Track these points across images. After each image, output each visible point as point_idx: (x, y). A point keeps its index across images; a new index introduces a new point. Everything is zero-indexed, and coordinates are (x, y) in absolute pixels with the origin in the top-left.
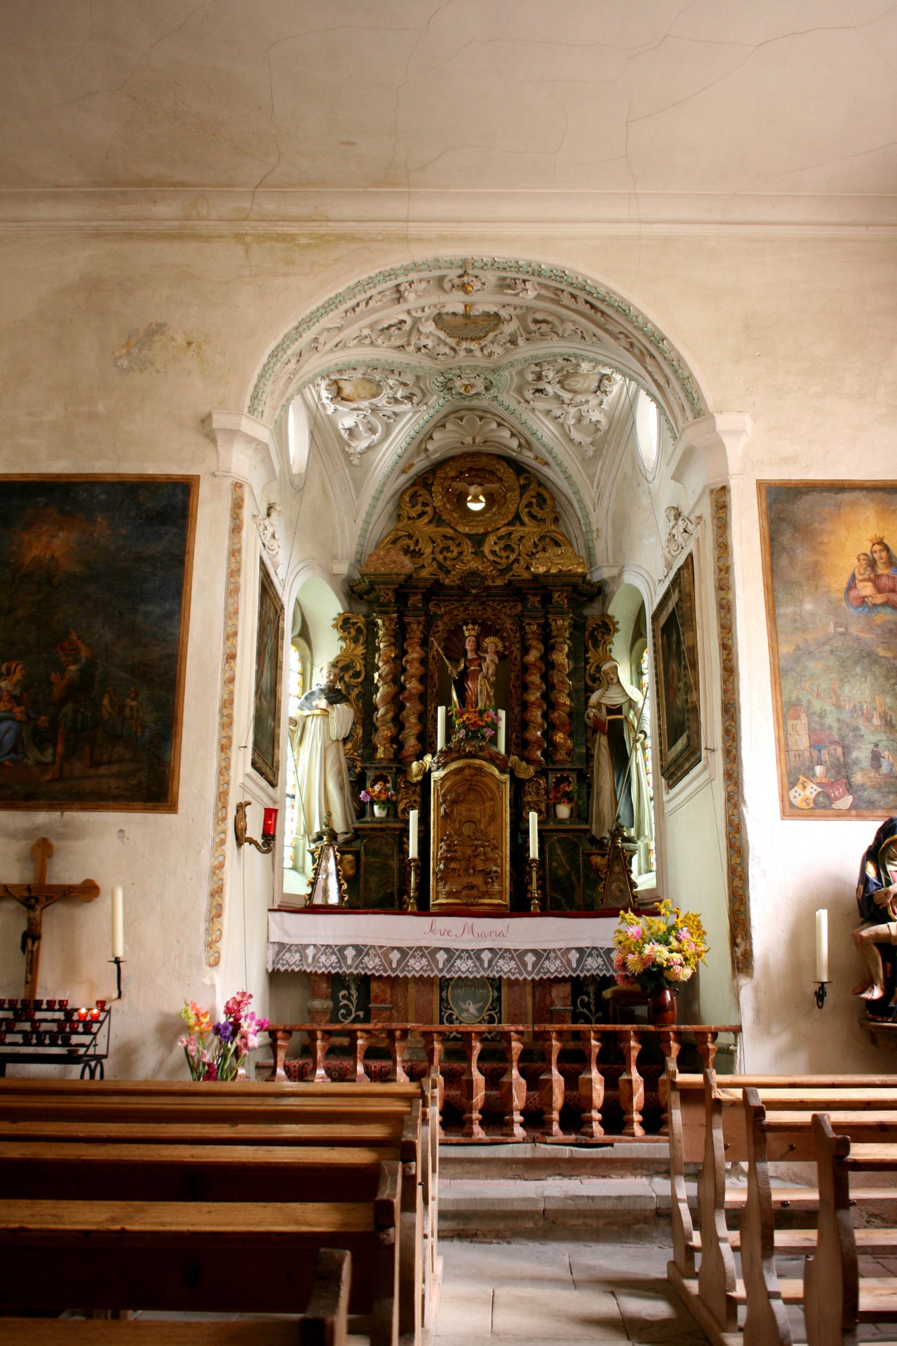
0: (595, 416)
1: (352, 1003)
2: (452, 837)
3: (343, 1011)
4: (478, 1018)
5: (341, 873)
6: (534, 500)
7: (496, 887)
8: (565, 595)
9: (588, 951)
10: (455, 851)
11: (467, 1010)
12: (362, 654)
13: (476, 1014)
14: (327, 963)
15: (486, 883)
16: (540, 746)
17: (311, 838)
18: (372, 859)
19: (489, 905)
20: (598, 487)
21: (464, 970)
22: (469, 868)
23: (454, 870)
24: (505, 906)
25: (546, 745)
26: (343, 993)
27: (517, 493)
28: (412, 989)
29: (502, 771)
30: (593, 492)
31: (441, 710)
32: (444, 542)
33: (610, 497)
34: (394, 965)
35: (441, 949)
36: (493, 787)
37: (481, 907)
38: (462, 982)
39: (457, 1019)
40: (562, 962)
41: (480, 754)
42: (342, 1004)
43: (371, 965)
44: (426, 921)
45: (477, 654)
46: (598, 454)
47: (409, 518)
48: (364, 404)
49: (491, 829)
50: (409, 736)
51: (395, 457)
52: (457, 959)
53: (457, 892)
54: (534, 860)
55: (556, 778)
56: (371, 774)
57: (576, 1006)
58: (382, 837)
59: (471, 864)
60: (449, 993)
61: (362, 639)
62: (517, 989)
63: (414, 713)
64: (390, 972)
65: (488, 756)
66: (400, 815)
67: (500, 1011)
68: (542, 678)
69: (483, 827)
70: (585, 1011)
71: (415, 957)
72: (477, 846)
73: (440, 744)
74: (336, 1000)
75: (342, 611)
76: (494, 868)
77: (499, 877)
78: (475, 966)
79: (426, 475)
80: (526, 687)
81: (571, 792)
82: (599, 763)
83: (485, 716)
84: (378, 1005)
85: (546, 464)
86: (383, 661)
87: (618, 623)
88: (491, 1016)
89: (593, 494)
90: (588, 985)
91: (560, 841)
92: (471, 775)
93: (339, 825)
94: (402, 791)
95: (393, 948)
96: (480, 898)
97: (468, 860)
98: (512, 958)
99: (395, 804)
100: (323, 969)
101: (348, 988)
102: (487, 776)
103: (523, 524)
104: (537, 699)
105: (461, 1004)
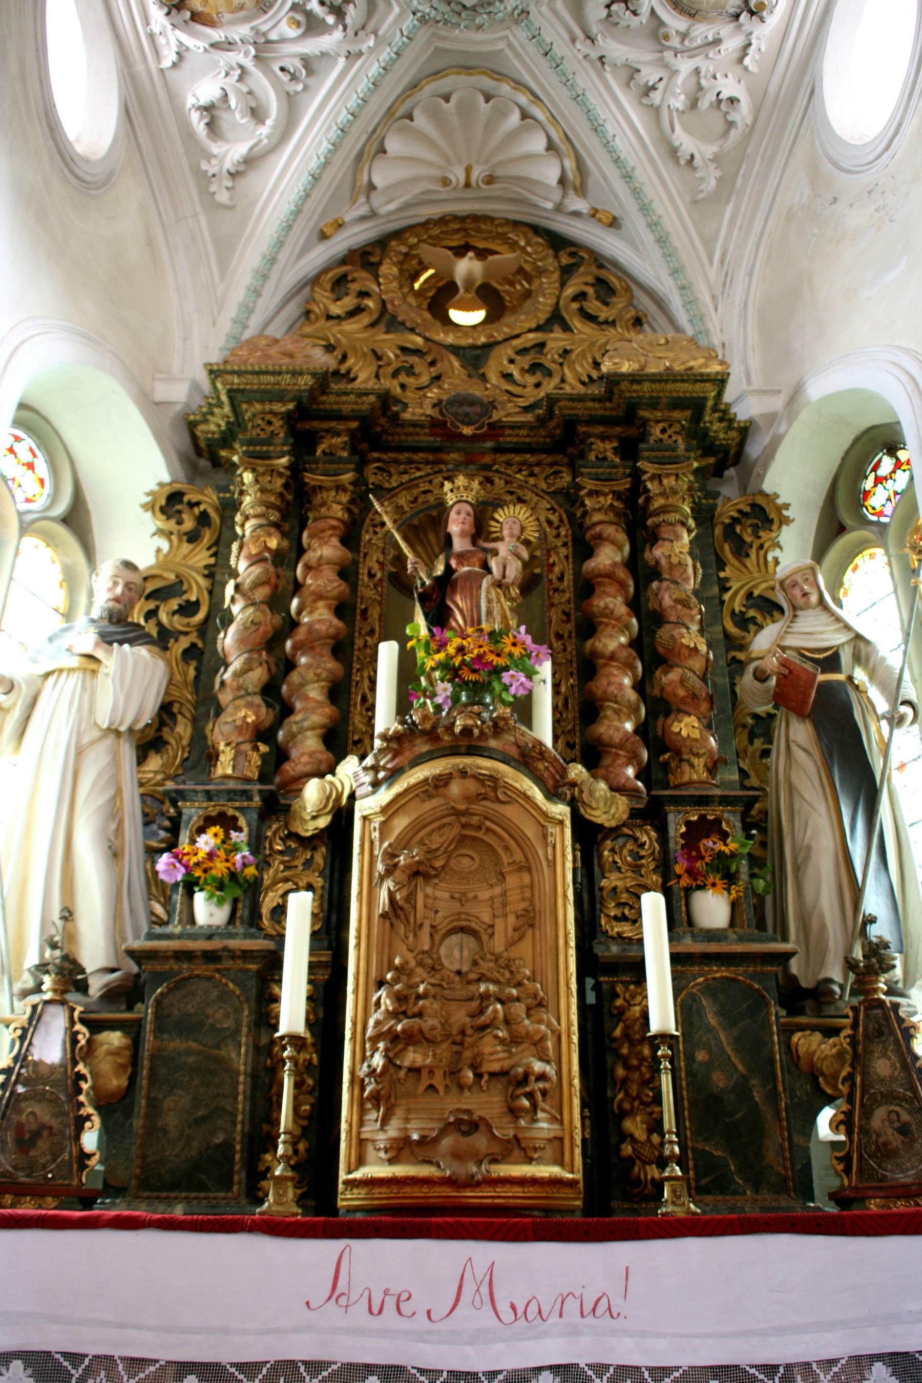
0: (729, 87)
2: (410, 974)
6: (590, 291)
7: (544, 1126)
8: (677, 427)
10: (420, 1015)
12: (207, 567)
15: (514, 1112)
16: (633, 758)
17: (18, 986)
18: (175, 1044)
19: (522, 1182)
20: (722, 262)
22: (460, 1062)
23: (415, 1071)
24: (572, 1184)
25: (645, 755)
27: (556, 275)
29: (552, 795)
30: (713, 273)
31: (387, 653)
32: (403, 358)
33: (750, 275)
36: (531, 832)
37: (500, 1190)
41: (493, 743)
44: (323, 1251)
45: (474, 543)
46: (726, 186)
47: (329, 317)
48: (241, 31)
49: (524, 949)
50: (302, 730)
51: (305, 179)
54: (664, 1037)
55: (688, 824)
56: (192, 812)
58: (209, 979)
59: (468, 1054)
61: (207, 537)
63: (319, 678)
65: (514, 752)
66: (266, 922)
68: (628, 604)
69: (498, 944)
72: (485, 997)
73: (385, 719)
75: (167, 478)
76: (538, 1067)
77: (554, 1093)
79: (369, 249)
81: (733, 855)
82: (791, 789)
83: (507, 641)
85: (614, 223)
86: (249, 557)
87: (787, 506)
89: (712, 276)
91: (710, 989)
92: (469, 799)
93: (95, 953)
94: (277, 864)
96: (495, 1161)
97: (459, 1040)
99: (254, 889)
102: (510, 801)
103: (567, 328)
104: (622, 646)
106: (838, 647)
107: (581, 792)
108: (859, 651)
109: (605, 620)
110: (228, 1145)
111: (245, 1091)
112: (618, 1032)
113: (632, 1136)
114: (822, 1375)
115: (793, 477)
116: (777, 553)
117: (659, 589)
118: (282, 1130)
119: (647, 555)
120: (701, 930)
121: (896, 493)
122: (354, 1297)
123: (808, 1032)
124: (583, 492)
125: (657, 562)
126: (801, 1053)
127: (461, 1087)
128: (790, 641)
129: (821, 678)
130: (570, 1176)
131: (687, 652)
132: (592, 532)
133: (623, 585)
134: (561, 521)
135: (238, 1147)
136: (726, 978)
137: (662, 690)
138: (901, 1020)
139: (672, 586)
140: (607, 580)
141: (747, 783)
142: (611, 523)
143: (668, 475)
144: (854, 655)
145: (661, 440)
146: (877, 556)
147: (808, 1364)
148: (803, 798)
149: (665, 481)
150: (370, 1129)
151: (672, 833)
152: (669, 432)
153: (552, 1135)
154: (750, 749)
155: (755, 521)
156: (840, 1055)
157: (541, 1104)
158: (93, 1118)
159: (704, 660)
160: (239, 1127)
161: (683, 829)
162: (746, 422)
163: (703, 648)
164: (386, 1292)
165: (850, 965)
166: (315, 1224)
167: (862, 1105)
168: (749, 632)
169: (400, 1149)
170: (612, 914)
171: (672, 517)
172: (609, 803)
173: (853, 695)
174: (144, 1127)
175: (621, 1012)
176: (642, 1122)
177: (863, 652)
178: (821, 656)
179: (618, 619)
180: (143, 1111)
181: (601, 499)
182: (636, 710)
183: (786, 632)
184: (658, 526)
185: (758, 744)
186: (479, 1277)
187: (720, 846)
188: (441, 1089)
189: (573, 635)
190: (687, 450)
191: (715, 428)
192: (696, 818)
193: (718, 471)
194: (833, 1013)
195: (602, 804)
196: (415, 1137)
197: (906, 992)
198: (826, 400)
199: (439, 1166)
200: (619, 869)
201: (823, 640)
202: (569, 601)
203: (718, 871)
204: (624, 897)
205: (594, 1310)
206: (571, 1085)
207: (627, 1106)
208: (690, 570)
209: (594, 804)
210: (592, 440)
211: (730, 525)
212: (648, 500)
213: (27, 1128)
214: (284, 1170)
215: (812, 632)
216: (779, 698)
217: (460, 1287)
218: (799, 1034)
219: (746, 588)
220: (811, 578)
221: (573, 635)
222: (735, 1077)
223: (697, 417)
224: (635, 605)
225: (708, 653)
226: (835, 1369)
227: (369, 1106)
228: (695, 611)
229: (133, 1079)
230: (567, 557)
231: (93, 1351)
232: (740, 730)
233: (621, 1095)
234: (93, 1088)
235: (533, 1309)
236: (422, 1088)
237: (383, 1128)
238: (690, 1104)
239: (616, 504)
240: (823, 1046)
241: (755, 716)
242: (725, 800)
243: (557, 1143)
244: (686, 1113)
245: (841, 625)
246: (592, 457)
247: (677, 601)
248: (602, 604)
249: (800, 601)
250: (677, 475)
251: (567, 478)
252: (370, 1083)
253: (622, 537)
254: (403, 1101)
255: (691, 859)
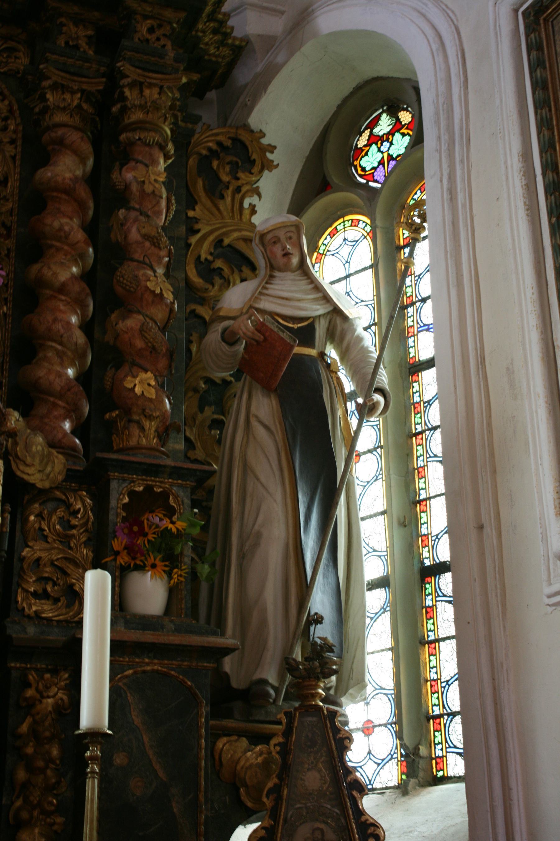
8: (167, 30)
16: (72, 411)
54: (94, 735)
55: (132, 494)
80: (34, 248)
81: (179, 535)
82: (246, 468)
87: (272, 148)
104: (73, 276)
106: (314, 318)
107: (16, 444)
108: (335, 327)
109: (58, 244)
112: (24, 728)
115: (283, 117)
116: (254, 200)
117: (125, 218)
119: (115, 176)
120: (135, 615)
121: (390, 158)
123: (234, 738)
124: (46, 83)
125: (127, 187)
126: (224, 761)
128: (265, 304)
129: (298, 350)
131: (150, 299)
132: (53, 135)
133: (82, 206)
134: (11, 111)
136: (157, 671)
137: (117, 337)
138: (336, 730)
139: (143, 218)
140: (64, 196)
141: (191, 454)
142: (76, 128)
143: (150, 86)
144: (328, 329)
145: (147, 41)
146: (361, 225)
148: (258, 479)
149: (147, 92)
151: (113, 503)
152: (158, 33)
154: (200, 417)
155: (235, 159)
156: (266, 764)
159: (168, 310)
161: (126, 500)
162: (242, 40)
163: (169, 297)
165: (288, 665)
168: (213, 285)
170: (32, 589)
171: (152, 137)
172: (46, 460)
173: (323, 373)
175: (31, 704)
176: (41, 834)
177: (339, 328)
178: (296, 326)
179: (73, 245)
181: (68, 96)
182: (83, 356)
183: (261, 293)
184: (132, 144)
185: (209, 412)
187: (166, 523)
189: (13, 254)
190: (176, 60)
191: (207, 40)
192: (141, 488)
193: (198, 91)
194: (262, 718)
195: (37, 461)
197: (338, 701)
198: (336, 35)
200: (45, 538)
201: (300, 309)
202: (11, 212)
203: (159, 551)
204: (48, 571)
207: (25, 815)
208: (164, 203)
209: (29, 460)
210: (63, 20)
211: (206, 156)
212: (124, 110)
215: (286, 298)
216: (245, 368)
218: (225, 739)
219: (216, 234)
220: (295, 237)
221: (13, 254)
223: (190, 24)
224: (92, 230)
225: (173, 303)
228: (163, 253)
230: (14, 158)
232: (190, 394)
239: (85, 106)
240: (249, 753)
241: (209, 381)
242: (176, 473)
245: (320, 295)
246: (61, 42)
247: (146, 237)
248: (56, 224)
249: (281, 261)
250: (161, 88)
251: (22, 61)
253: (87, 148)
255: (131, 534)
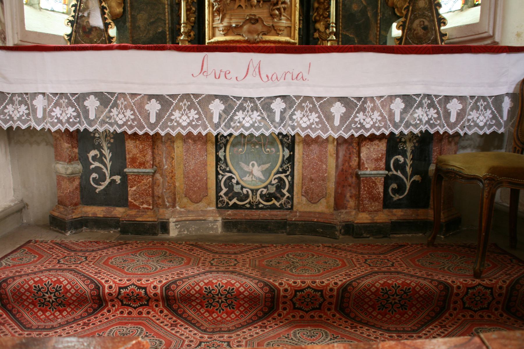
1: (105, 165)
3: (94, 175)
4: (263, 182)
5: (106, 12)
7: (284, 22)
9: (418, 100)
11: (251, 173)
13: (262, 177)
14: (63, 118)
15: (272, 16)
19: (274, 42)
21: (247, 125)
26: (93, 153)
28: (179, 148)
34: (153, 120)
35: (216, 96)
38: (244, 140)
39: (238, 183)
40: (381, 115)
42: (92, 166)
43: (121, 119)
44: (198, 56)
52: (238, 110)
53: (237, 27)
57: (388, 168)
60: (228, 153)
62: (315, 148)
64: (147, 129)
67: (292, 175)
70: (399, 174)
71: (180, 109)
74: (86, 163)
78: (263, 118)
84: (136, 170)
88: (280, 179)
90: (405, 142)
95: (151, 97)
98: (313, 109)
100: (59, 126)
101: (99, 147)
105: (243, 165)
110: (163, 33)
111: (168, 12)
113: (319, 30)
114: (377, 101)
118: (182, 22)
122: (209, 73)
127: (252, 6)
130: (293, 41)
135: (167, 33)
147: (373, 97)
150: (217, 23)
153: (287, 25)
157: (283, 13)
158: (111, 24)
160: (167, 25)
164: (221, 71)
166: (193, 47)
167: (410, 19)
169: (228, 30)
174: (131, 26)
176: (323, 24)
180: (130, 20)
186: (255, 66)
188: (244, 7)
196: (234, 25)
199: (243, 36)
205: (297, 78)
206: (295, 6)
207: (318, 18)
213: (86, 27)
214: (184, 37)
217: (248, 69)
222: (362, 6)
226: (382, 99)
227: (216, 14)
229: (124, 9)
231: (118, 91)
233: (315, 14)
234: (110, 12)
235: (274, 77)
236: (236, 6)
237: (221, 23)
238: (343, 16)
243: (289, 29)
244: (341, 20)
252: (216, 5)
254: (229, 12)
